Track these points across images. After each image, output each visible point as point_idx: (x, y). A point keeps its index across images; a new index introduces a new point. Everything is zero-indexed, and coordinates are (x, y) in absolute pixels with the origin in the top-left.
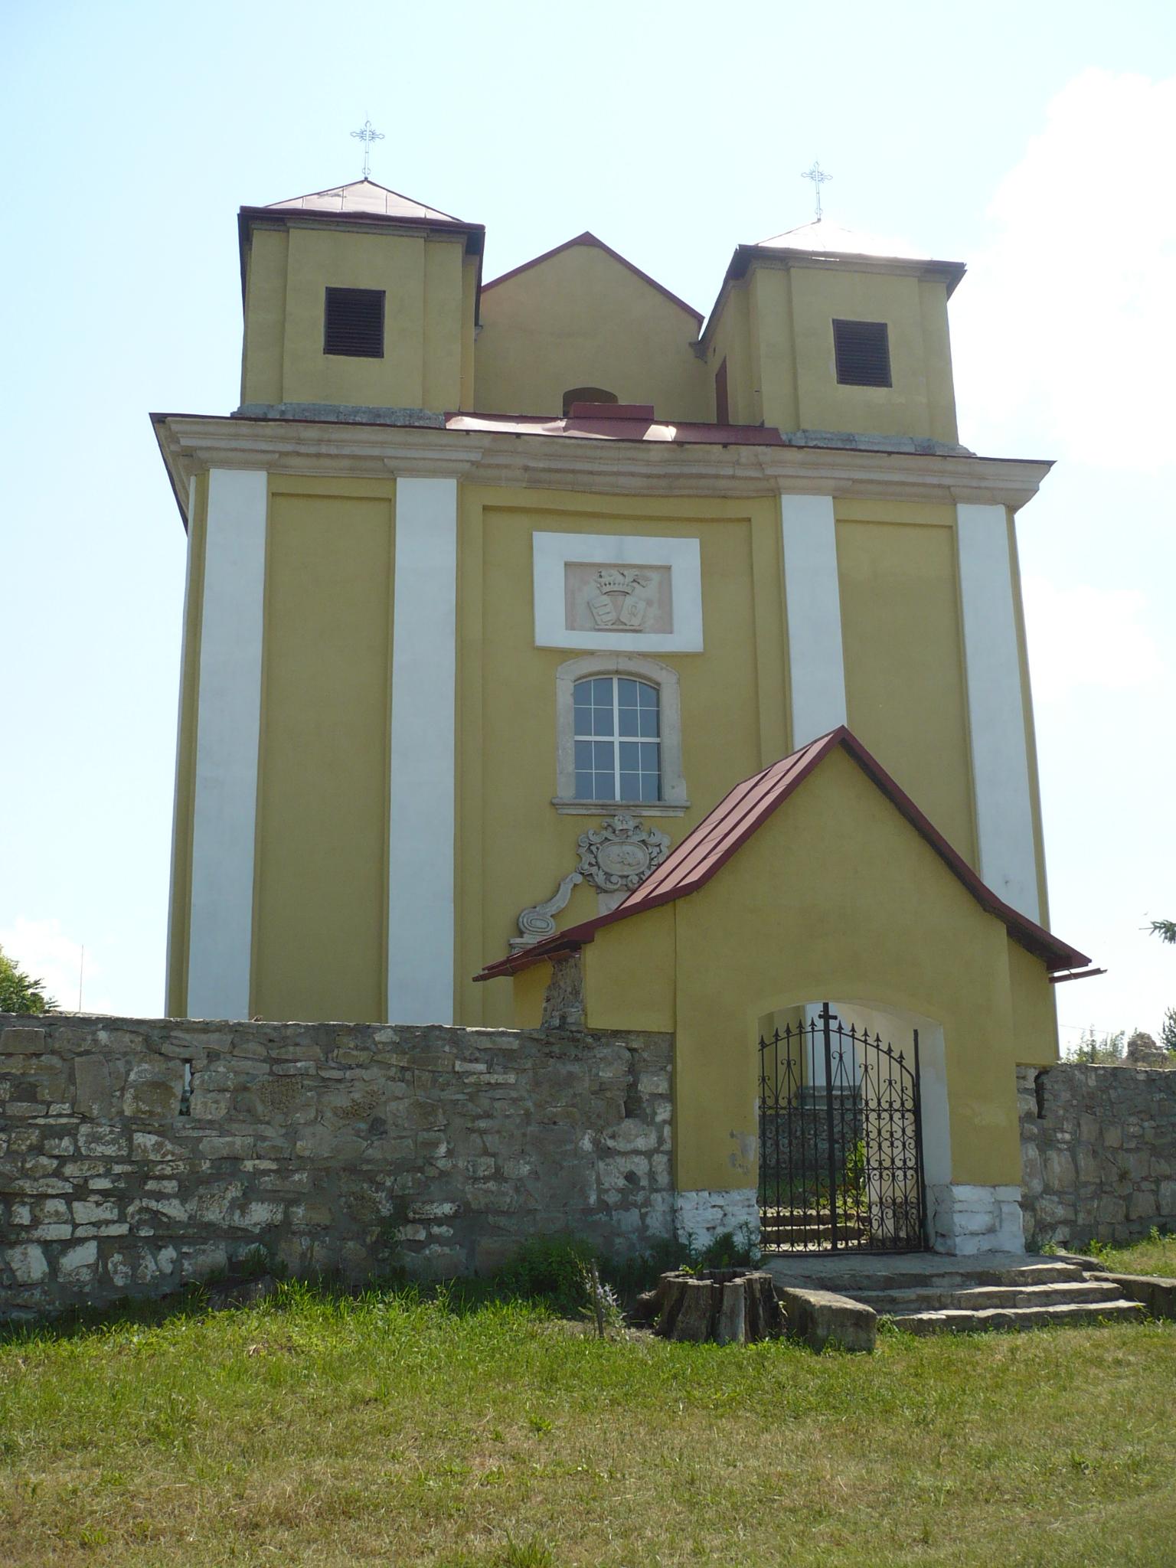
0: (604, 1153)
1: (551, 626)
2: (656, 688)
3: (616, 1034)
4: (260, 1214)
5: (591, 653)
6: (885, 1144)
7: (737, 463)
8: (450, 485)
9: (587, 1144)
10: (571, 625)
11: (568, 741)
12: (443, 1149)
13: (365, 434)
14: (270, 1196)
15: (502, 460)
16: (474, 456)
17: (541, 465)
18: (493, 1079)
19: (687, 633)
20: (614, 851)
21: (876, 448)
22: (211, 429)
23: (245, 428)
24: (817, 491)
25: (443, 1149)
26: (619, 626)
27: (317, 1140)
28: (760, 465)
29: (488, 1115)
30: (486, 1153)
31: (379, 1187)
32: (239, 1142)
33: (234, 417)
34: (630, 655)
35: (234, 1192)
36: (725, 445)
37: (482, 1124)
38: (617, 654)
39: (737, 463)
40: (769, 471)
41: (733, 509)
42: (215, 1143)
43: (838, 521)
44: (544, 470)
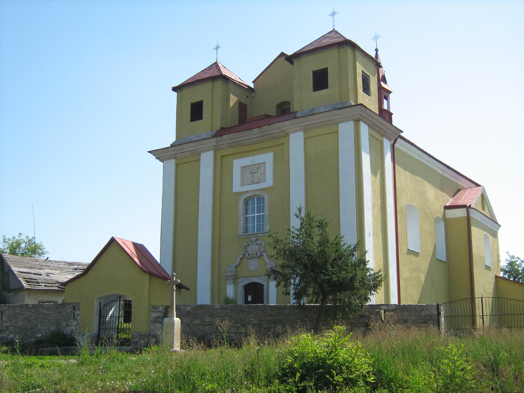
0: (68, 325)
1: (237, 187)
2: (263, 199)
3: (71, 303)
4: (12, 336)
5: (247, 192)
6: (519, 322)
7: (274, 129)
8: (302, 132)
9: (64, 324)
10: (242, 185)
11: (266, 213)
12: (39, 325)
13: (189, 145)
14: (13, 333)
15: (221, 143)
16: (214, 144)
17: (230, 142)
18: (48, 312)
19: (269, 182)
20: (250, 247)
21: (203, 142)
22: (160, 152)
23: (172, 148)
24: (298, 131)
25: (39, 325)
26: (253, 183)
27: (20, 324)
28: (279, 128)
29: (46, 319)
30: (46, 326)
31: (29, 331)
32: (9, 324)
33: (172, 146)
34: (257, 190)
35: (8, 332)
36: (269, 125)
37: (46, 321)
38: (253, 191)
39: (274, 129)
40: (283, 129)
41: (281, 141)
42: (5, 324)
43: (338, 132)
44: (232, 143)
